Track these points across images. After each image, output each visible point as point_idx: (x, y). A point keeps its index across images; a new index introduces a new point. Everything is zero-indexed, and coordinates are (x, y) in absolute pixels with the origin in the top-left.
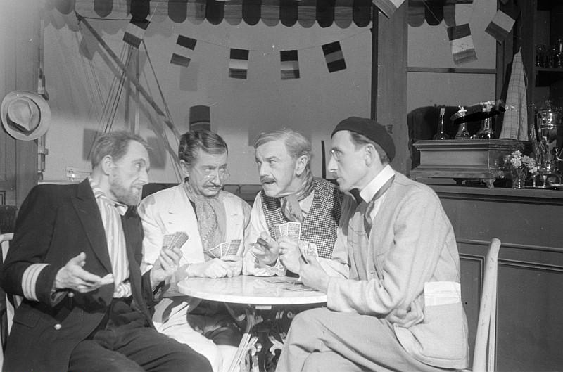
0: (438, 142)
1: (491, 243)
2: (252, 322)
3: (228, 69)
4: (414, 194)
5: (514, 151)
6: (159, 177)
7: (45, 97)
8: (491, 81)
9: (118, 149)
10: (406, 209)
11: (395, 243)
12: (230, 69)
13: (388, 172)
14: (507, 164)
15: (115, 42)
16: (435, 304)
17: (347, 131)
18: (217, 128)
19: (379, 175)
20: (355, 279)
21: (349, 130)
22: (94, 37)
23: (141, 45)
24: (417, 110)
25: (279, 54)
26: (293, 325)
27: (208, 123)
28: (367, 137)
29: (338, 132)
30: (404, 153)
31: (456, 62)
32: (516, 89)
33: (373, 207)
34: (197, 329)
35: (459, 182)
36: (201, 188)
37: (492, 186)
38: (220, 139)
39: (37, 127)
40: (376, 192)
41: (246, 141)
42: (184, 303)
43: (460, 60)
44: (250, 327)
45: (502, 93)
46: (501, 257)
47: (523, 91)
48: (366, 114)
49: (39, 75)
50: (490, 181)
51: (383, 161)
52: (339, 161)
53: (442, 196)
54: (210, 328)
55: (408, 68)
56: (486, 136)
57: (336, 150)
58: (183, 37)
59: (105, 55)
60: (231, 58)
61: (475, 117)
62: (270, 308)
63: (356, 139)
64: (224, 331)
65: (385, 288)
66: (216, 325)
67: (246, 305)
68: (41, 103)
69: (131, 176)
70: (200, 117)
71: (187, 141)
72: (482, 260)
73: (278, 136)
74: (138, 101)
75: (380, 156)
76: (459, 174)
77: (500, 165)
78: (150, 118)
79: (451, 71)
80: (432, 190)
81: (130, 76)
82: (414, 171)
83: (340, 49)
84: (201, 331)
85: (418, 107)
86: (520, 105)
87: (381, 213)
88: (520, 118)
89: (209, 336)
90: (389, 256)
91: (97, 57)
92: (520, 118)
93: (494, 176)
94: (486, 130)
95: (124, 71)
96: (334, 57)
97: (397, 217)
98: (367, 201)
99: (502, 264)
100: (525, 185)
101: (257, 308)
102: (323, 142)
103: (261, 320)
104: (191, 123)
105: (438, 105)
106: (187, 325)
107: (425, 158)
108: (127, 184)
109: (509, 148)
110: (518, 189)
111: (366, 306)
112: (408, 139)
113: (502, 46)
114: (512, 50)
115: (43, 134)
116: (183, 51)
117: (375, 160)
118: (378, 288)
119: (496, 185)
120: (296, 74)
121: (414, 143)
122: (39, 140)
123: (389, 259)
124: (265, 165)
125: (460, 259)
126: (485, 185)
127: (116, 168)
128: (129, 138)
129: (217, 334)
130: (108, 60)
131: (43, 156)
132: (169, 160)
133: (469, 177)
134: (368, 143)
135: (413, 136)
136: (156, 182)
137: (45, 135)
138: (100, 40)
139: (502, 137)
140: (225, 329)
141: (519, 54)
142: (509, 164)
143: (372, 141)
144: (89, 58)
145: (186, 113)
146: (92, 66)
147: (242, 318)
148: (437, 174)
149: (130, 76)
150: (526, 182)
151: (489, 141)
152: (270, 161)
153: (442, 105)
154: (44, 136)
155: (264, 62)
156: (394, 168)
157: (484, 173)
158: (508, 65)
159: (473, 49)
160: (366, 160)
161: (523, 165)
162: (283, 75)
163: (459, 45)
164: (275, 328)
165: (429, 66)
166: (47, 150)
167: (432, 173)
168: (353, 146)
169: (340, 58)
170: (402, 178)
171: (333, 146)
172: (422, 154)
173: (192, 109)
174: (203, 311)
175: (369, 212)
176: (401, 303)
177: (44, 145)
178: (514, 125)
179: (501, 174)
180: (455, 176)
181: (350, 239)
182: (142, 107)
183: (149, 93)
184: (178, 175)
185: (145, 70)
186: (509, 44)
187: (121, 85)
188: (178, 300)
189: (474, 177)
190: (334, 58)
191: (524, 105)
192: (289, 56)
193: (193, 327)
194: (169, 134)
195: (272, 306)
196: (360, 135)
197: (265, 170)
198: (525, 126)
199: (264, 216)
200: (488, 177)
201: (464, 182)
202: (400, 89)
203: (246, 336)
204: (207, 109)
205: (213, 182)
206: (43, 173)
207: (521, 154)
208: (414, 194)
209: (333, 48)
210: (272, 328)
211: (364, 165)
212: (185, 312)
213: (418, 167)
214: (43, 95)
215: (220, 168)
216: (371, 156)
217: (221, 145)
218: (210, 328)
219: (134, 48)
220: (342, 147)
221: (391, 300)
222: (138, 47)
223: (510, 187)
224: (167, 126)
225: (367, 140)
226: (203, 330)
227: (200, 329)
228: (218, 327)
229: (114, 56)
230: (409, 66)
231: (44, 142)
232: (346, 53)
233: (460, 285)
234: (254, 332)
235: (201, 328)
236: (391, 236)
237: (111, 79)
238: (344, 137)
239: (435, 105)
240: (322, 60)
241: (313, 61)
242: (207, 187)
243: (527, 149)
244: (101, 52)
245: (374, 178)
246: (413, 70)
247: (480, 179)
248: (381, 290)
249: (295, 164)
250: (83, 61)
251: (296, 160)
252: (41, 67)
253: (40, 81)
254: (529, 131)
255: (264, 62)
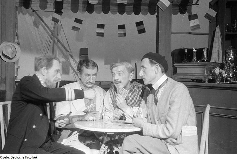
0: (185, 64)
1: (206, 107)
2: (106, 140)
3: (96, 33)
4: (178, 87)
5: (216, 68)
6: (66, 78)
7: (18, 44)
8: (206, 38)
9: (49, 65)
10: (174, 94)
11: (170, 108)
12: (97, 32)
13: (164, 77)
14: (213, 73)
15: (48, 21)
16: (186, 136)
17: (147, 59)
18: (92, 58)
19: (161, 78)
20: (150, 123)
21: (148, 58)
22: (39, 19)
23: (59, 22)
24: (175, 50)
25: (135, 24)
26: (124, 142)
28: (156, 61)
29: (144, 59)
30: (171, 68)
31: (192, 30)
32: (217, 41)
33: (158, 93)
34: (82, 142)
35: (193, 80)
36: (85, 84)
37: (207, 82)
38: (94, 63)
39: (15, 57)
40: (160, 85)
41: (103, 63)
42: (76, 132)
43: (193, 29)
44: (105, 142)
45: (211, 42)
46: (211, 112)
47: (220, 42)
48: (154, 51)
49: (16, 35)
50: (206, 80)
51: (162, 72)
52: (144, 71)
53: (188, 86)
54: (88, 142)
55: (172, 32)
56: (204, 61)
57: (143, 67)
58: (77, 19)
59: (44, 26)
60: (97, 28)
61: (200, 52)
62: (113, 134)
63: (151, 62)
64: (94, 143)
65: (167, 128)
66: (90, 140)
67: (103, 132)
68: (17, 46)
69: (54, 76)
70: (84, 52)
71: (81, 64)
72: (202, 113)
73: (122, 64)
74: (58, 46)
75: (162, 69)
76: (193, 77)
77: (210, 73)
78: (63, 53)
79: (190, 33)
80: (183, 84)
81: (54, 35)
82: (174, 76)
83: (143, 24)
84: (84, 143)
85: (176, 48)
86: (219, 48)
87: (163, 95)
88: (219, 53)
89: (87, 145)
90: (168, 114)
91: (40, 27)
92: (219, 53)
93: (208, 78)
94: (205, 58)
95: (52, 33)
96: (141, 27)
97: (171, 97)
98: (155, 90)
99: (211, 115)
100: (221, 82)
101: (108, 133)
102: (136, 63)
103: (109, 139)
104: (80, 55)
105: (184, 48)
106: (78, 141)
107: (179, 70)
108: (52, 80)
109: (214, 66)
110: (218, 84)
111: (159, 135)
112: (172, 63)
113: (211, 23)
114: (215, 25)
115: (17, 59)
116: (77, 25)
117: (159, 71)
118: (164, 127)
120: (125, 35)
121: (174, 64)
122: (16, 62)
123: (168, 115)
124: (117, 75)
125: (196, 113)
126: (204, 82)
127: (48, 73)
128: (53, 59)
129: (91, 144)
130: (46, 29)
131: (18, 69)
132: (71, 71)
133: (197, 78)
134: (157, 64)
135: (174, 61)
136: (65, 80)
137: (18, 60)
138: (42, 20)
139: (211, 61)
140: (94, 142)
141: (218, 26)
142: (214, 73)
143: (158, 63)
144: (36, 27)
145: (78, 51)
146: (38, 31)
147: (101, 138)
148: (184, 77)
149: (54, 35)
150: (221, 80)
151: (206, 63)
153: (186, 48)
154: (18, 61)
155: (111, 30)
156: (167, 75)
157: (204, 77)
158: (214, 31)
159: (199, 25)
160: (155, 71)
161: (220, 74)
162: (119, 35)
163: (193, 23)
164: (116, 142)
165: (178, 32)
166: (19, 66)
167: (182, 77)
168: (150, 65)
169: (143, 28)
170: (170, 80)
171: (141, 65)
172: (177, 68)
173: (81, 49)
174: (85, 134)
175: (156, 94)
176: (174, 134)
177: (18, 64)
178: (216, 56)
179: (211, 77)
180: (191, 78)
181: (148, 106)
182: (59, 48)
183: (62, 42)
184: (74, 77)
185: (61, 33)
186: (214, 22)
187: (51, 39)
188: (73, 130)
189: (199, 78)
190: (140, 27)
191: (221, 48)
192: (122, 27)
193: (81, 142)
194: (71, 60)
195: (114, 132)
196: (153, 61)
197: (117, 77)
198: (221, 56)
199: (109, 93)
201: (195, 81)
202: (168, 41)
203: (103, 145)
204: (87, 49)
205: (89, 80)
206: (18, 76)
207: (219, 69)
208: (178, 87)
209: (139, 24)
210: (114, 142)
211: (155, 74)
212: (78, 135)
213: (176, 74)
214: (18, 43)
215: (93, 75)
216: (158, 70)
217: (95, 65)
218: (88, 142)
219: (56, 23)
220: (145, 66)
221: (169, 132)
222: (58, 23)
223: (215, 82)
224: (70, 56)
225: (156, 62)
226: (85, 143)
227: (84, 142)
228: (91, 141)
229: (48, 27)
230: (172, 31)
231: (18, 63)
232: (146, 26)
233: (197, 127)
234: (106, 144)
235: (84, 142)
236: (168, 106)
237: (46, 36)
238: (147, 61)
239: (183, 48)
240: (135, 29)
241: (131, 29)
242: (87, 83)
243: (222, 67)
244: (42, 25)
245: (158, 80)
246: (174, 33)
247: (202, 79)
248: (165, 129)
249: (129, 75)
250: (35, 29)
251: (130, 74)
252: (17, 31)
253: (16, 37)
254: (223, 59)
255: (111, 30)
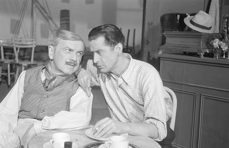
18: (73, 22)
27: (68, 18)
37: (202, 57)
104: (61, 17)
107: (168, 40)
119: (204, 56)
142: (212, 46)
152: (98, 52)
200: (201, 52)
213: (165, 45)
